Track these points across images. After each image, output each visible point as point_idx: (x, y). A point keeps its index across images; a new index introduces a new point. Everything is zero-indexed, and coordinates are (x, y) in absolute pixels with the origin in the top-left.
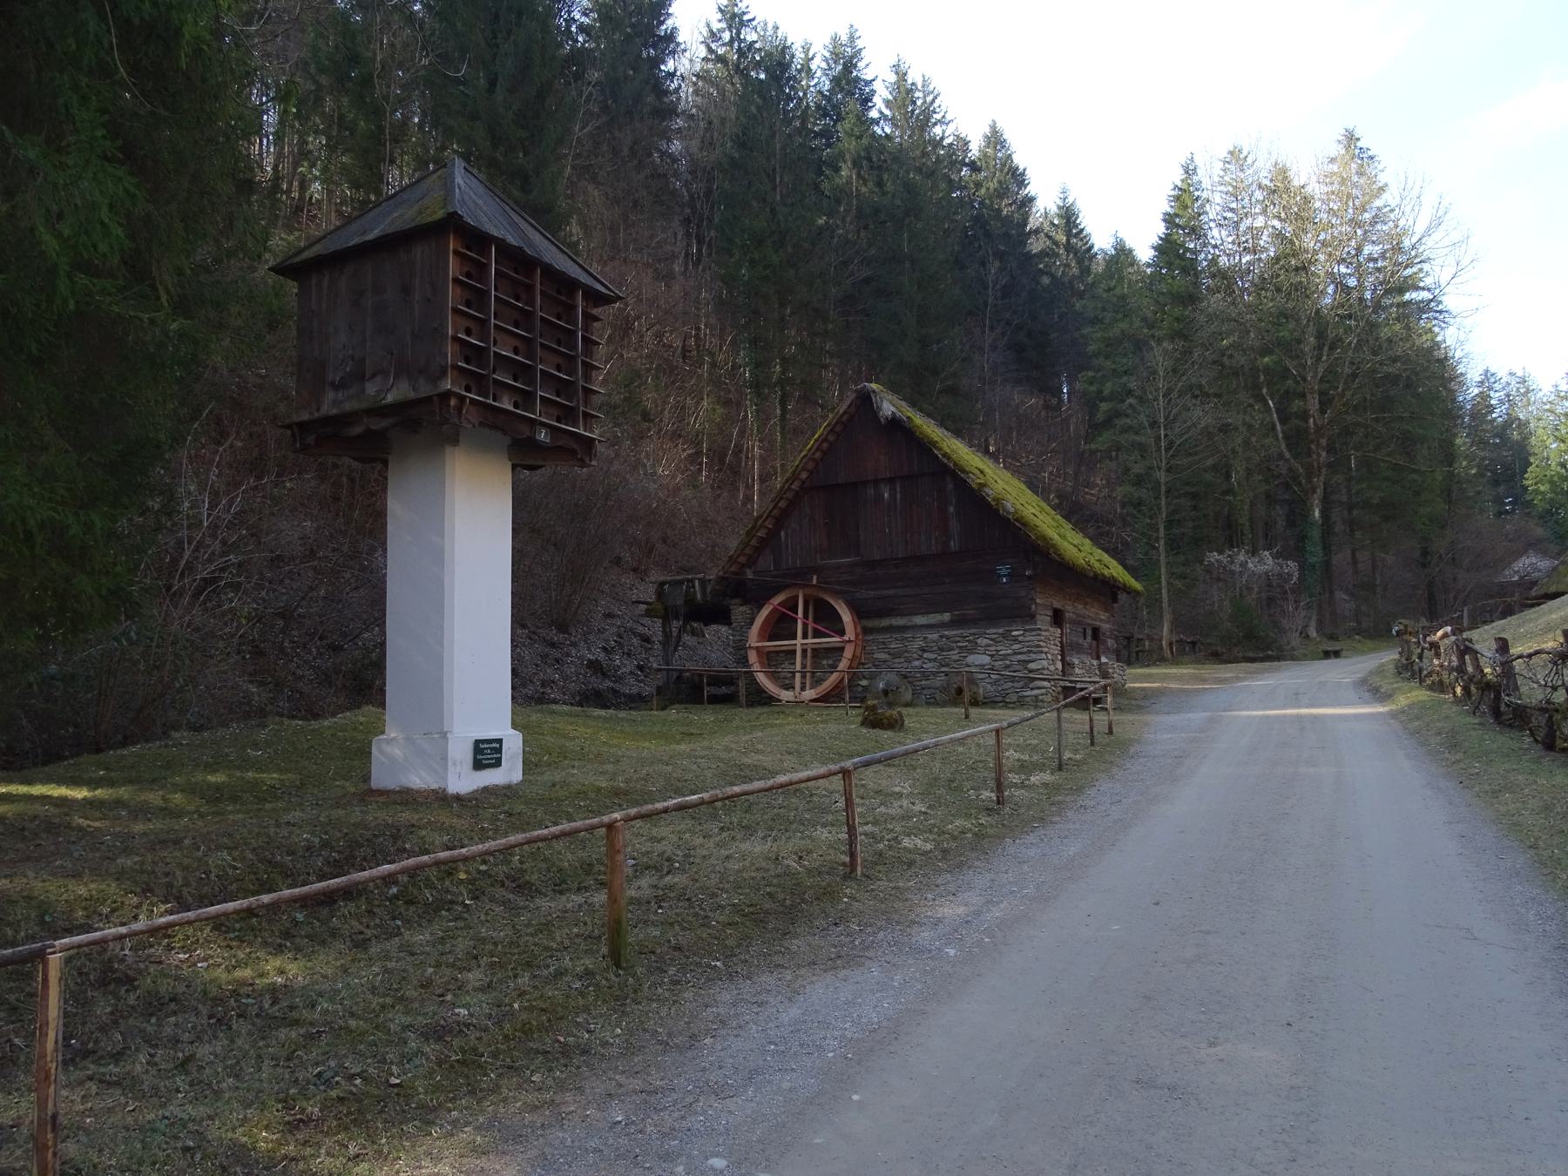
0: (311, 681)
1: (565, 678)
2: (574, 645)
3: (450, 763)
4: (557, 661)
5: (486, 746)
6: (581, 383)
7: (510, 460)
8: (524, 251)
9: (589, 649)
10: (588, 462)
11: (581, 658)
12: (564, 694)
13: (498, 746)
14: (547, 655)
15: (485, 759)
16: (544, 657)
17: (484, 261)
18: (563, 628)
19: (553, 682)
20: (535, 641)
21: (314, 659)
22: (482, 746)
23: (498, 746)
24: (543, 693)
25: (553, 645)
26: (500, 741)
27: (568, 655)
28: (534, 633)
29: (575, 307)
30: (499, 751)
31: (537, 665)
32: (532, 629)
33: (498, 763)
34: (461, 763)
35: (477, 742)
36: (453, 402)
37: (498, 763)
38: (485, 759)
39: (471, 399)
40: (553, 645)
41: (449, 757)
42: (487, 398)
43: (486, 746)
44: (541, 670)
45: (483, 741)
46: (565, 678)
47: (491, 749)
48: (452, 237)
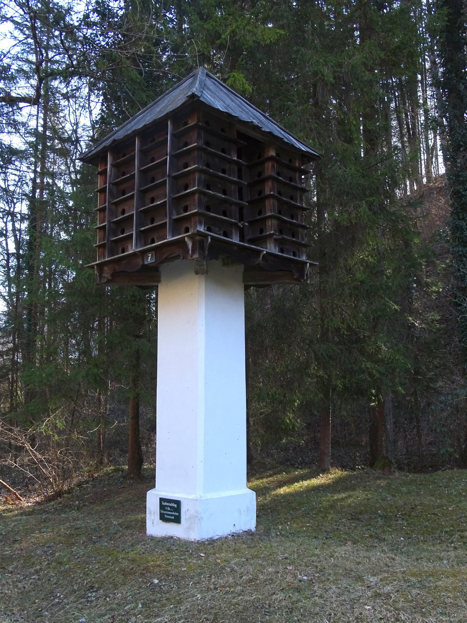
13: (175, 506)
23: (175, 506)
47: (170, 507)
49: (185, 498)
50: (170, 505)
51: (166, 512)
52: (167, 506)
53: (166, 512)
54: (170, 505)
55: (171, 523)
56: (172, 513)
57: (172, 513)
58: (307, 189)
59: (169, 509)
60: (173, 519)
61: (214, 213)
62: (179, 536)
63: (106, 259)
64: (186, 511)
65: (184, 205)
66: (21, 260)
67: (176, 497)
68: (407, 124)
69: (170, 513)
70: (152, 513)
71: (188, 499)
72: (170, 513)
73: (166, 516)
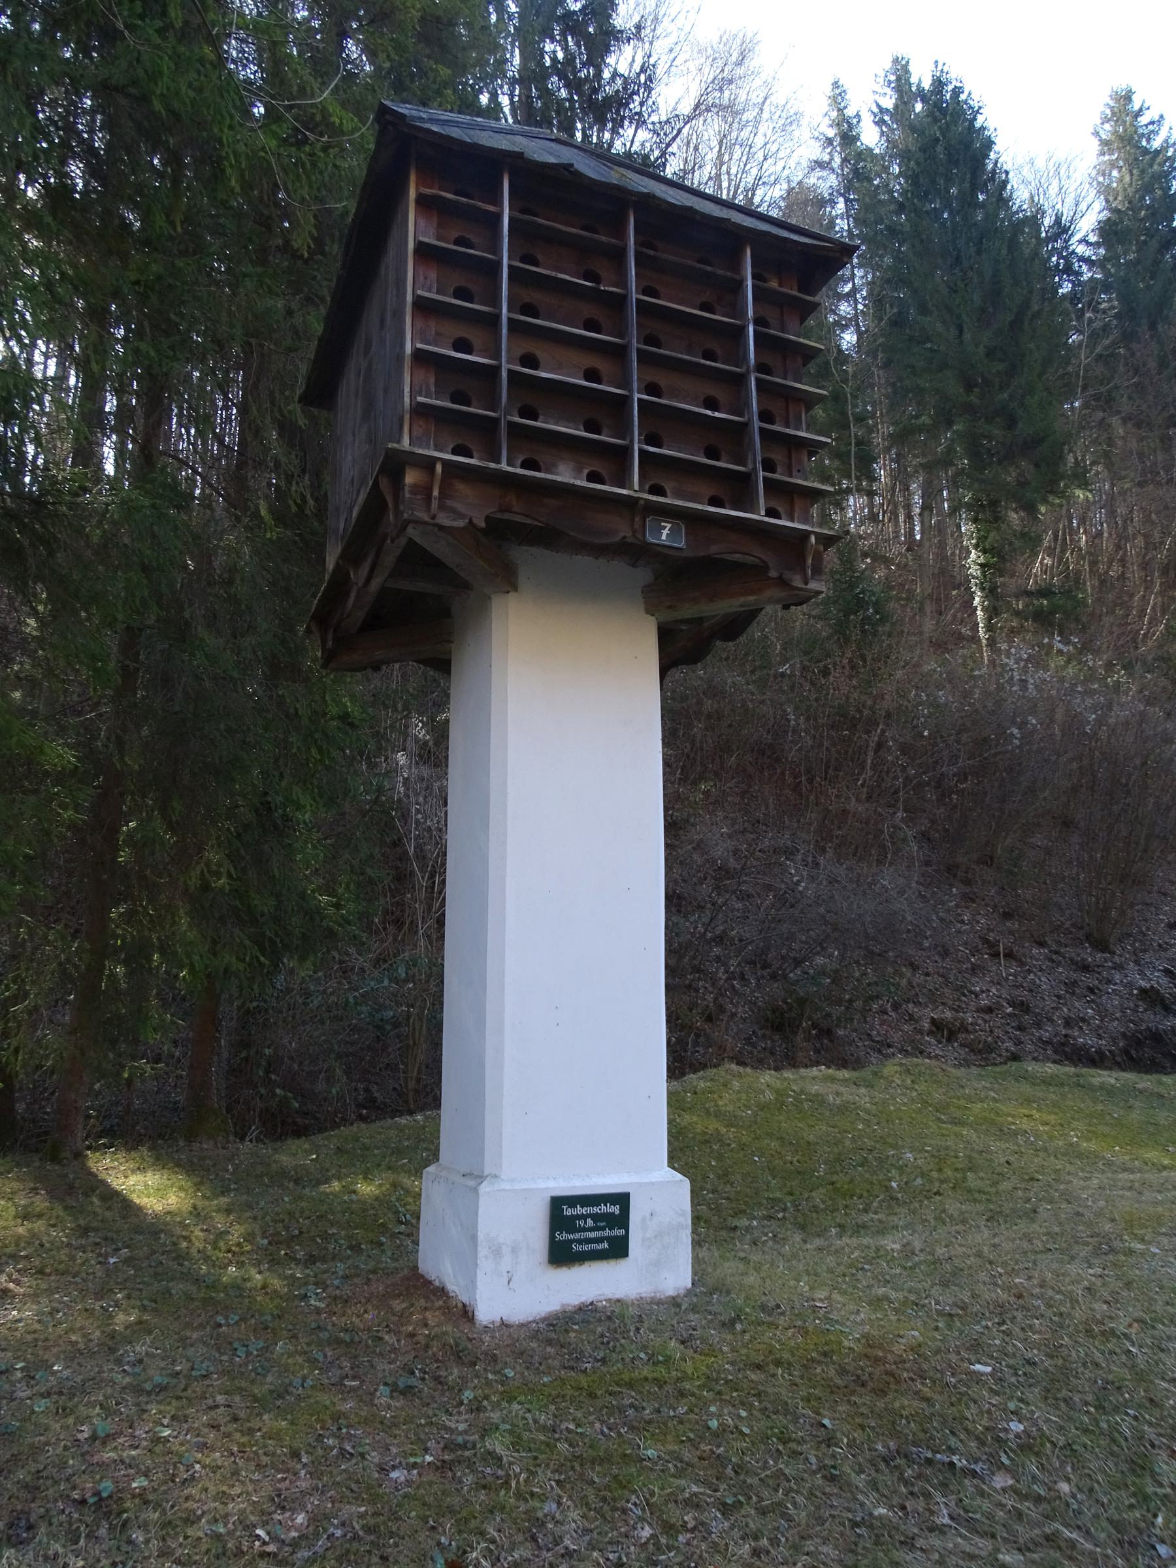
0: (745, 1020)
1: (1103, 1014)
2: (1119, 967)
3: (483, 1251)
4: (1091, 990)
5: (579, 1210)
6: (757, 424)
7: (649, 612)
8: (578, 174)
9: (1141, 973)
10: (797, 582)
11: (1130, 985)
12: (1100, 1037)
13: (616, 1210)
14: (1075, 983)
15: (580, 1242)
16: (1071, 985)
17: (491, 208)
18: (1102, 946)
19: (1083, 1020)
20: (1059, 964)
21: (753, 992)
22: (568, 1212)
23: (616, 1210)
24: (1066, 1036)
25: (1086, 968)
26: (622, 1200)
27: (1109, 982)
28: (1057, 953)
29: (741, 283)
30: (622, 1220)
31: (1059, 997)
32: (1054, 947)
33: (619, 1249)
34: (515, 1251)
35: (557, 1203)
36: (411, 477)
37: (619, 1249)
38: (580, 1242)
39: (445, 463)
40: (1086, 968)
41: (481, 1236)
42: (499, 462)
43: (579, 1210)
44: (1065, 1004)
45: (573, 1201)
46: (1103, 1014)
47: (595, 1217)
48: (413, 178)
49: (640, 1184)
50: (596, 1210)
51: (577, 1236)
52: (584, 1217)
53: (577, 1236)
54: (596, 1210)
55: (587, 1264)
56: (601, 1234)
57: (601, 1234)
58: (376, 107)
59: (590, 1222)
60: (603, 1250)
61: (470, 255)
62: (619, 1293)
63: (578, 483)
64: (644, 1220)
65: (780, 509)
66: (99, 117)
67: (610, 1186)
68: (909, 517)
69: (592, 1235)
70: (506, 1250)
71: (653, 1184)
72: (592, 1235)
73: (576, 1247)
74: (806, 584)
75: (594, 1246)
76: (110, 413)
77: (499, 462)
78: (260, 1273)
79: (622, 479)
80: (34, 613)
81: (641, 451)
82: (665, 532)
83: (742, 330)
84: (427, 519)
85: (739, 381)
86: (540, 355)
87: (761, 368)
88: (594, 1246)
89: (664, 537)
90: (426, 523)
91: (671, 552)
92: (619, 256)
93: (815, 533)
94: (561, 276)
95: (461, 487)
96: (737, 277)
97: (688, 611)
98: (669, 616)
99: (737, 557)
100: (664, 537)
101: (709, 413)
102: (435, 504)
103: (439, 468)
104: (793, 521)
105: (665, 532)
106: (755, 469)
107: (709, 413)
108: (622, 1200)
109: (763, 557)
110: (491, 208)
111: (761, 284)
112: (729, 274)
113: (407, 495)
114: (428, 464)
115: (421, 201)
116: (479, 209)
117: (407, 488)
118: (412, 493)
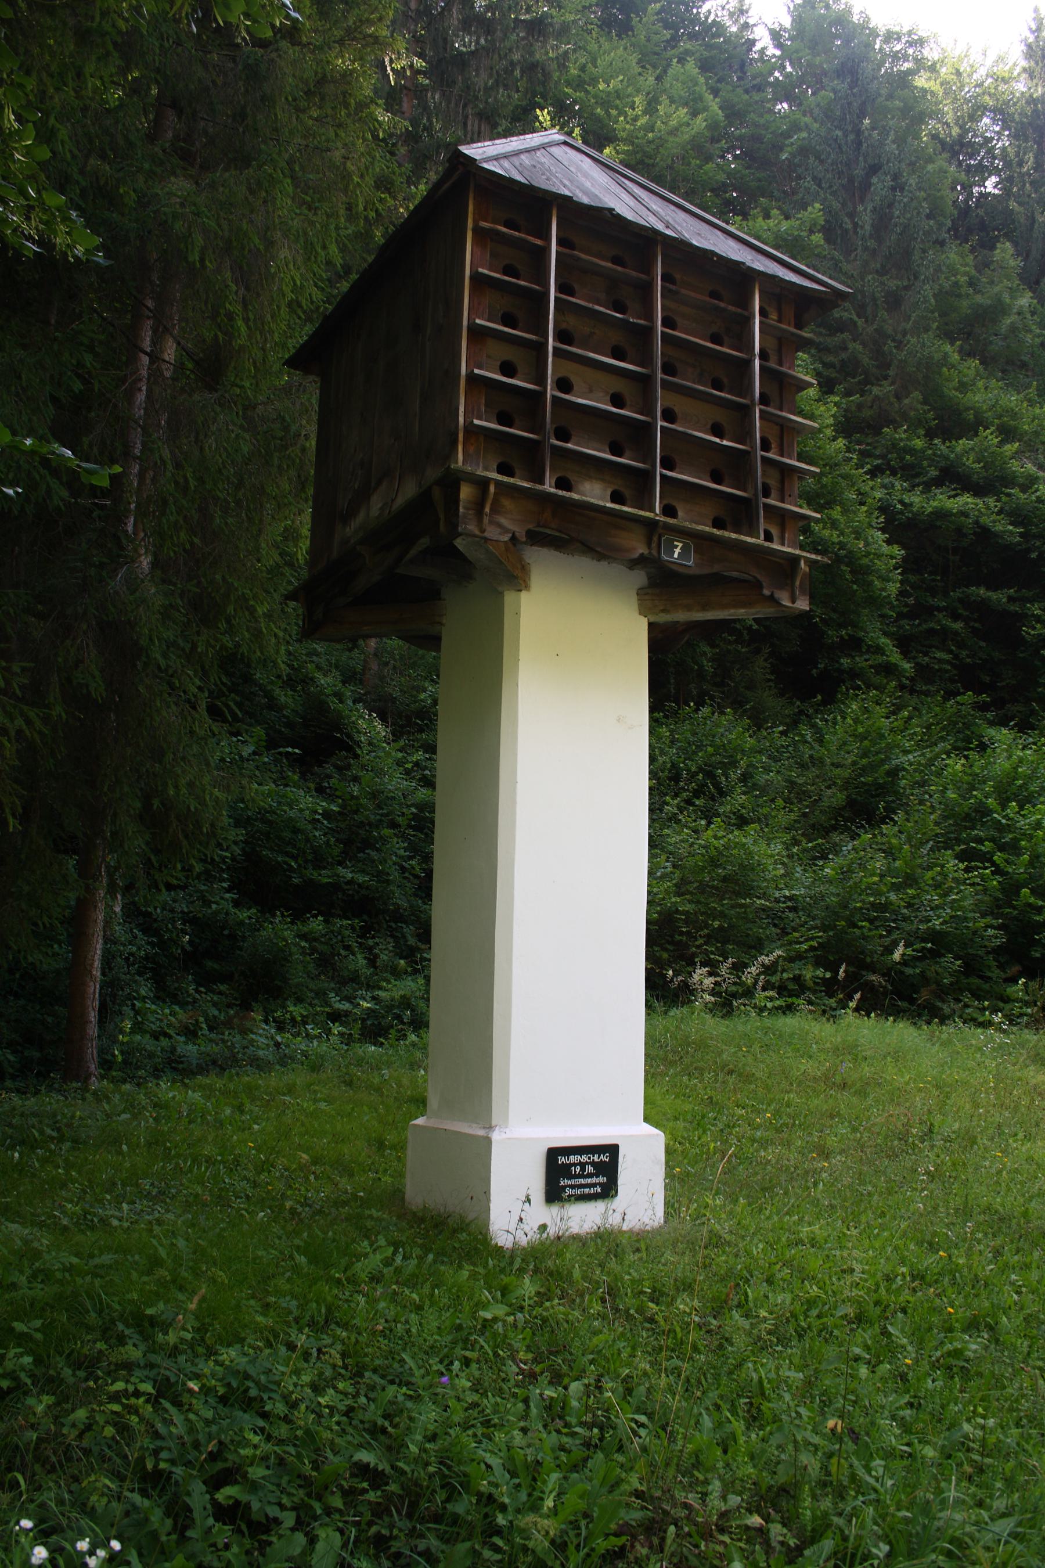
8: (619, 217)
13: (605, 1158)
15: (572, 1187)
17: (539, 242)
23: (605, 1158)
26: (613, 1150)
38: (572, 1187)
51: (573, 1182)
53: (573, 1182)
74: (793, 602)
75: (587, 1190)
76: (149, 318)
77: (542, 483)
78: (19, 119)
79: (644, 499)
80: (364, 1491)
81: (662, 475)
82: (677, 551)
83: (748, 363)
84: (477, 532)
85: (745, 411)
86: (575, 380)
87: (764, 400)
88: (587, 1190)
89: (676, 555)
90: (475, 536)
91: (681, 570)
92: (646, 291)
93: (806, 559)
94: (597, 308)
95: (507, 503)
96: (746, 313)
97: (681, 616)
98: (663, 618)
99: (735, 574)
100: (676, 555)
101: (717, 440)
102: (486, 520)
103: (492, 489)
104: (783, 544)
105: (677, 551)
106: (756, 495)
107: (717, 440)
108: (613, 1150)
109: (758, 577)
110: (539, 242)
111: (671, 286)
112: (739, 310)
113: (461, 510)
114: (483, 484)
115: (477, 230)
116: (527, 242)
117: (461, 504)
118: (465, 508)
